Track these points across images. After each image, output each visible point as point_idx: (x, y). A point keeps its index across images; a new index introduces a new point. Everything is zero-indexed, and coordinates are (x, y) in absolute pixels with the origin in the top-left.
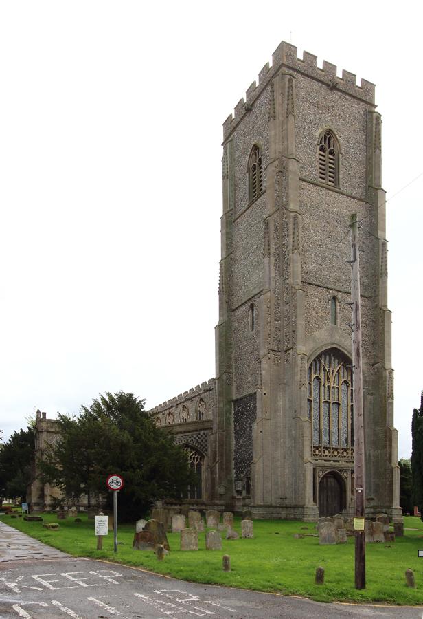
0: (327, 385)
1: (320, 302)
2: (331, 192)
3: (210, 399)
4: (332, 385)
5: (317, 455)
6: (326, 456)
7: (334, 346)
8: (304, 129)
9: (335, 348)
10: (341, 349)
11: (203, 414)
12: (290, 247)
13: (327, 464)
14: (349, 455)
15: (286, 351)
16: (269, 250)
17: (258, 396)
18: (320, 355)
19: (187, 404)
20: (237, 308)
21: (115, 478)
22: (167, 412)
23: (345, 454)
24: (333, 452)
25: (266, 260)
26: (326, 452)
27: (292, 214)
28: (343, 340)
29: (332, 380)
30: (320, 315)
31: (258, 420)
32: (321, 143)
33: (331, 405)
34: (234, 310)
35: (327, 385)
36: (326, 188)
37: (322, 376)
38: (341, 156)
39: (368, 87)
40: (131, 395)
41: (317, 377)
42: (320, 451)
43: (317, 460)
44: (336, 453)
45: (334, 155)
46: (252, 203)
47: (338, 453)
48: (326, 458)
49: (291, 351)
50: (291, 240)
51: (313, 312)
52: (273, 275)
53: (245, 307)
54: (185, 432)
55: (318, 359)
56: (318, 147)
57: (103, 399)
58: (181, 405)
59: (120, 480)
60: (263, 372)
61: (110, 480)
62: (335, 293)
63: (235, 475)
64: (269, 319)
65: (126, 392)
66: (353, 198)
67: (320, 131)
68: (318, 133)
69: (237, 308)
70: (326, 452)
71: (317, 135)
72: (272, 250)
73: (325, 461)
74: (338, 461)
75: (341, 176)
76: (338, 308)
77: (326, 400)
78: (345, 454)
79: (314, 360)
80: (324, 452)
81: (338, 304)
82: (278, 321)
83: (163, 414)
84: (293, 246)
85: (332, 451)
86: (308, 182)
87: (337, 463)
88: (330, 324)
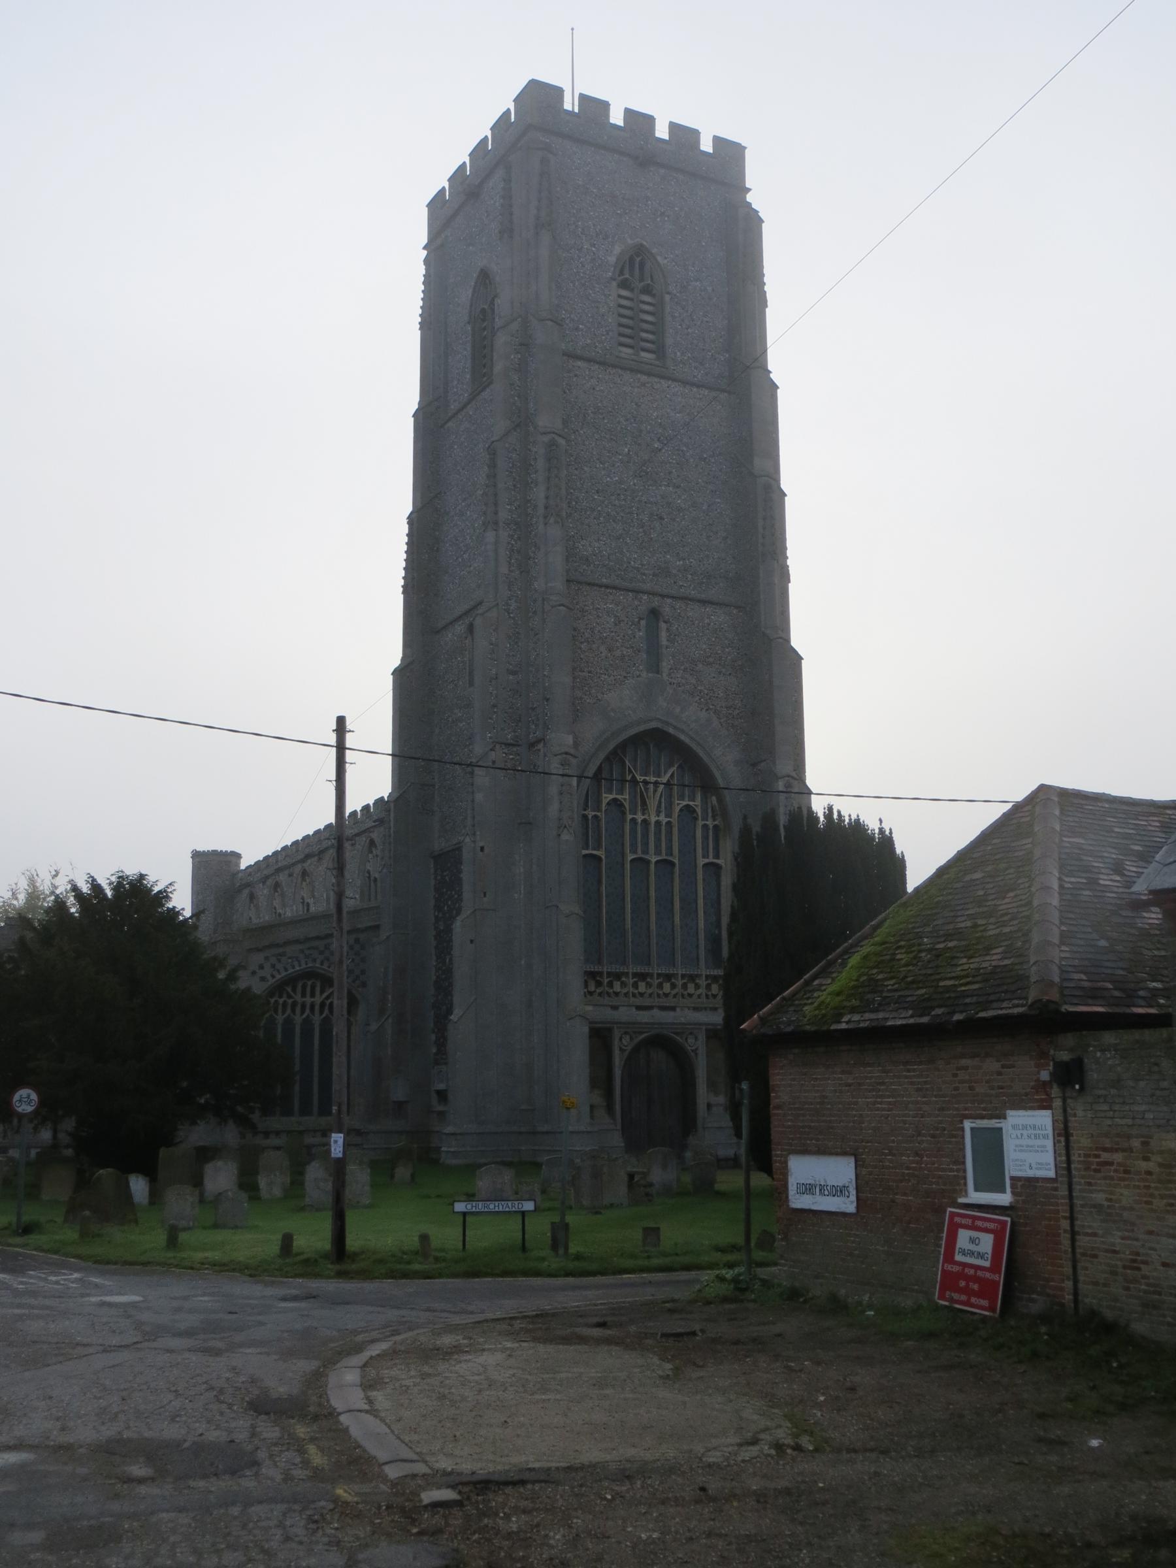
0: (640, 817)
1: (618, 622)
2: (644, 378)
3: (322, 871)
4: (653, 819)
5: (617, 994)
6: (641, 995)
7: (654, 725)
8: (580, 250)
9: (656, 730)
10: (671, 731)
11: (375, 880)
12: (541, 511)
13: (644, 1017)
14: (702, 991)
15: (532, 745)
16: (496, 513)
17: (466, 855)
18: (623, 746)
19: (309, 865)
20: (445, 627)
21: (23, 1092)
22: (298, 869)
23: (691, 988)
24: (660, 986)
25: (490, 536)
26: (642, 987)
27: (546, 439)
28: (678, 710)
29: (652, 804)
30: (618, 653)
31: (466, 912)
32: (621, 273)
33: (652, 867)
34: (438, 632)
35: (640, 817)
36: (632, 370)
37: (625, 797)
38: (667, 297)
39: (730, 155)
40: (142, 877)
41: (615, 800)
42: (623, 984)
43: (615, 1008)
44: (667, 987)
45: (654, 296)
46: (474, 396)
47: (673, 986)
48: (639, 1001)
49: (540, 746)
50: (542, 495)
51: (602, 648)
52: (504, 569)
53: (460, 628)
54: (308, 939)
55: (616, 756)
56: (614, 284)
57: (75, 889)
58: (363, 839)
59: (34, 1096)
60: (479, 797)
61: (16, 1097)
62: (656, 602)
63: (434, 1050)
64: (494, 672)
65: (131, 871)
66: (698, 386)
67: (617, 250)
68: (614, 253)
69: (445, 627)
70: (642, 987)
71: (612, 259)
72: (503, 515)
73: (639, 1008)
74: (673, 1009)
75: (669, 341)
76: (664, 635)
77: (639, 854)
78: (691, 988)
79: (607, 759)
80: (635, 985)
81: (663, 626)
82: (514, 673)
83: (290, 875)
84: (546, 508)
85: (680, 983)
86: (589, 360)
87: (672, 1014)
88: (644, 674)
